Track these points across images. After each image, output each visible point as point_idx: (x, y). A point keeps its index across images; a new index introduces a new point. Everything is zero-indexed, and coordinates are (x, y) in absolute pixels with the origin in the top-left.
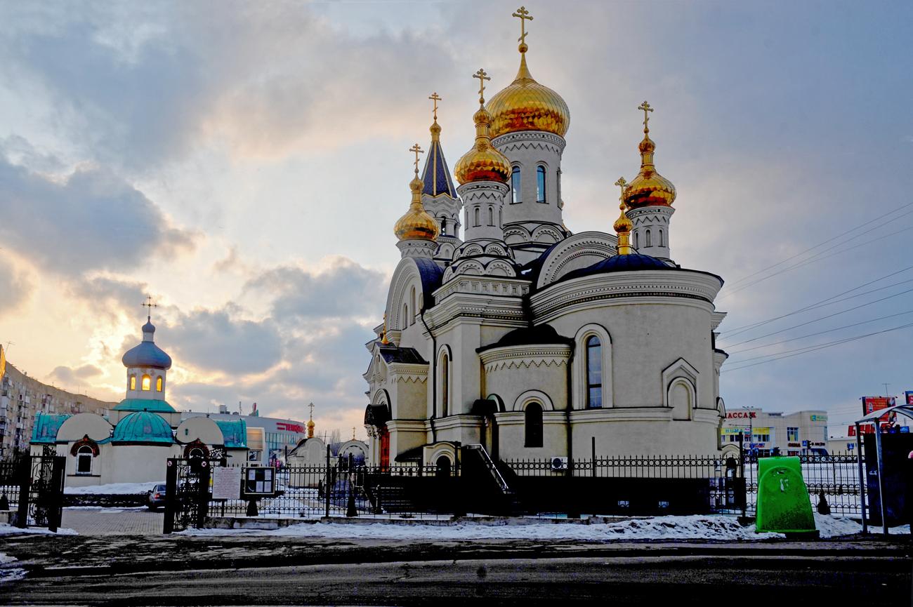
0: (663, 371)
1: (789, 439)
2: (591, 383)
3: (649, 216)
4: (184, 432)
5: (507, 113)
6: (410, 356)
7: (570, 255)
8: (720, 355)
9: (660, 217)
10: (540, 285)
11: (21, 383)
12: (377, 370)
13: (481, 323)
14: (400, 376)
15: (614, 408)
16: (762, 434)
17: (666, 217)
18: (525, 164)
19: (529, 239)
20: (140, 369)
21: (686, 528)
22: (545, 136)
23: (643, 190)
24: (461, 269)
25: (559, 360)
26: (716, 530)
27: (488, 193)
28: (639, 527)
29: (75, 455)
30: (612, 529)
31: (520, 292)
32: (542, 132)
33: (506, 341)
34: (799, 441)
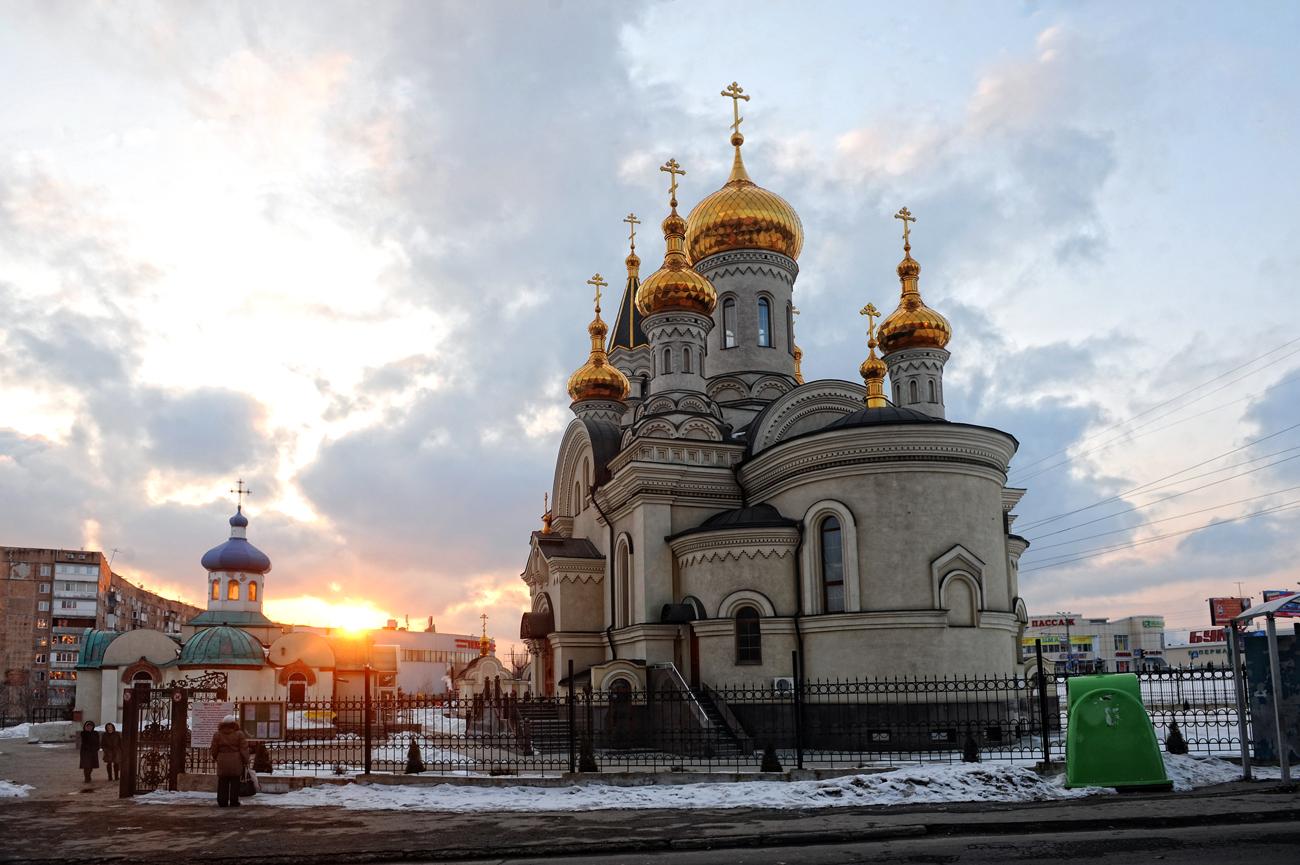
0: (932, 562)
1: (1116, 648)
2: (829, 580)
3: (914, 362)
4: (280, 653)
5: (716, 226)
6: (586, 550)
7: (801, 412)
8: (1017, 542)
9: (929, 363)
10: (757, 448)
11: (134, 599)
12: (536, 567)
13: (671, 503)
14: (564, 574)
15: (861, 612)
16: (1083, 643)
17: (938, 364)
18: (741, 295)
19: (746, 394)
20: (225, 573)
21: (948, 785)
22: (769, 257)
23: (904, 327)
24: (645, 431)
25: (781, 550)
26: (999, 788)
27: (682, 328)
28: (867, 787)
29: (285, 685)
30: (821, 791)
31: (728, 460)
32: (764, 251)
33: (709, 525)
34: (1130, 650)
